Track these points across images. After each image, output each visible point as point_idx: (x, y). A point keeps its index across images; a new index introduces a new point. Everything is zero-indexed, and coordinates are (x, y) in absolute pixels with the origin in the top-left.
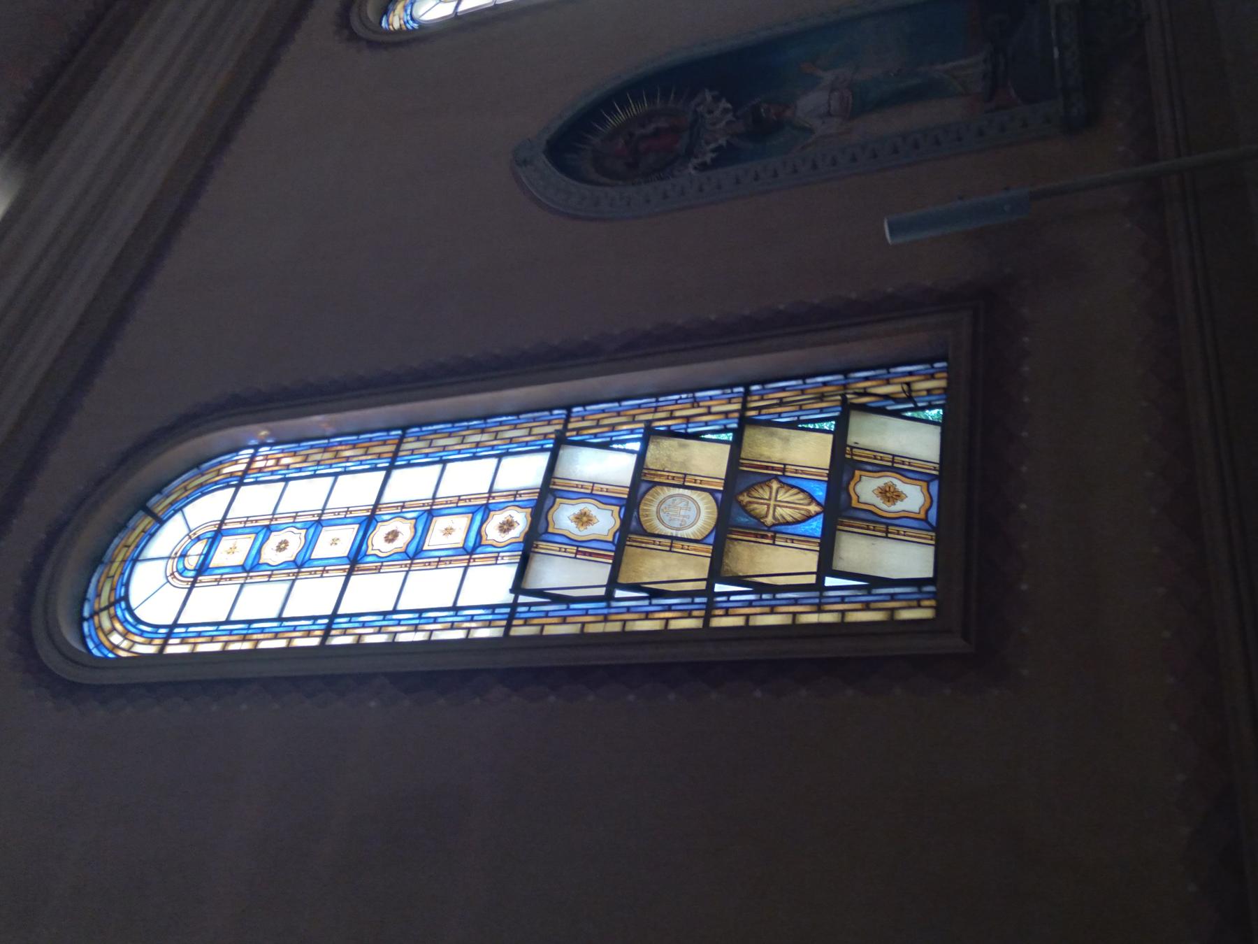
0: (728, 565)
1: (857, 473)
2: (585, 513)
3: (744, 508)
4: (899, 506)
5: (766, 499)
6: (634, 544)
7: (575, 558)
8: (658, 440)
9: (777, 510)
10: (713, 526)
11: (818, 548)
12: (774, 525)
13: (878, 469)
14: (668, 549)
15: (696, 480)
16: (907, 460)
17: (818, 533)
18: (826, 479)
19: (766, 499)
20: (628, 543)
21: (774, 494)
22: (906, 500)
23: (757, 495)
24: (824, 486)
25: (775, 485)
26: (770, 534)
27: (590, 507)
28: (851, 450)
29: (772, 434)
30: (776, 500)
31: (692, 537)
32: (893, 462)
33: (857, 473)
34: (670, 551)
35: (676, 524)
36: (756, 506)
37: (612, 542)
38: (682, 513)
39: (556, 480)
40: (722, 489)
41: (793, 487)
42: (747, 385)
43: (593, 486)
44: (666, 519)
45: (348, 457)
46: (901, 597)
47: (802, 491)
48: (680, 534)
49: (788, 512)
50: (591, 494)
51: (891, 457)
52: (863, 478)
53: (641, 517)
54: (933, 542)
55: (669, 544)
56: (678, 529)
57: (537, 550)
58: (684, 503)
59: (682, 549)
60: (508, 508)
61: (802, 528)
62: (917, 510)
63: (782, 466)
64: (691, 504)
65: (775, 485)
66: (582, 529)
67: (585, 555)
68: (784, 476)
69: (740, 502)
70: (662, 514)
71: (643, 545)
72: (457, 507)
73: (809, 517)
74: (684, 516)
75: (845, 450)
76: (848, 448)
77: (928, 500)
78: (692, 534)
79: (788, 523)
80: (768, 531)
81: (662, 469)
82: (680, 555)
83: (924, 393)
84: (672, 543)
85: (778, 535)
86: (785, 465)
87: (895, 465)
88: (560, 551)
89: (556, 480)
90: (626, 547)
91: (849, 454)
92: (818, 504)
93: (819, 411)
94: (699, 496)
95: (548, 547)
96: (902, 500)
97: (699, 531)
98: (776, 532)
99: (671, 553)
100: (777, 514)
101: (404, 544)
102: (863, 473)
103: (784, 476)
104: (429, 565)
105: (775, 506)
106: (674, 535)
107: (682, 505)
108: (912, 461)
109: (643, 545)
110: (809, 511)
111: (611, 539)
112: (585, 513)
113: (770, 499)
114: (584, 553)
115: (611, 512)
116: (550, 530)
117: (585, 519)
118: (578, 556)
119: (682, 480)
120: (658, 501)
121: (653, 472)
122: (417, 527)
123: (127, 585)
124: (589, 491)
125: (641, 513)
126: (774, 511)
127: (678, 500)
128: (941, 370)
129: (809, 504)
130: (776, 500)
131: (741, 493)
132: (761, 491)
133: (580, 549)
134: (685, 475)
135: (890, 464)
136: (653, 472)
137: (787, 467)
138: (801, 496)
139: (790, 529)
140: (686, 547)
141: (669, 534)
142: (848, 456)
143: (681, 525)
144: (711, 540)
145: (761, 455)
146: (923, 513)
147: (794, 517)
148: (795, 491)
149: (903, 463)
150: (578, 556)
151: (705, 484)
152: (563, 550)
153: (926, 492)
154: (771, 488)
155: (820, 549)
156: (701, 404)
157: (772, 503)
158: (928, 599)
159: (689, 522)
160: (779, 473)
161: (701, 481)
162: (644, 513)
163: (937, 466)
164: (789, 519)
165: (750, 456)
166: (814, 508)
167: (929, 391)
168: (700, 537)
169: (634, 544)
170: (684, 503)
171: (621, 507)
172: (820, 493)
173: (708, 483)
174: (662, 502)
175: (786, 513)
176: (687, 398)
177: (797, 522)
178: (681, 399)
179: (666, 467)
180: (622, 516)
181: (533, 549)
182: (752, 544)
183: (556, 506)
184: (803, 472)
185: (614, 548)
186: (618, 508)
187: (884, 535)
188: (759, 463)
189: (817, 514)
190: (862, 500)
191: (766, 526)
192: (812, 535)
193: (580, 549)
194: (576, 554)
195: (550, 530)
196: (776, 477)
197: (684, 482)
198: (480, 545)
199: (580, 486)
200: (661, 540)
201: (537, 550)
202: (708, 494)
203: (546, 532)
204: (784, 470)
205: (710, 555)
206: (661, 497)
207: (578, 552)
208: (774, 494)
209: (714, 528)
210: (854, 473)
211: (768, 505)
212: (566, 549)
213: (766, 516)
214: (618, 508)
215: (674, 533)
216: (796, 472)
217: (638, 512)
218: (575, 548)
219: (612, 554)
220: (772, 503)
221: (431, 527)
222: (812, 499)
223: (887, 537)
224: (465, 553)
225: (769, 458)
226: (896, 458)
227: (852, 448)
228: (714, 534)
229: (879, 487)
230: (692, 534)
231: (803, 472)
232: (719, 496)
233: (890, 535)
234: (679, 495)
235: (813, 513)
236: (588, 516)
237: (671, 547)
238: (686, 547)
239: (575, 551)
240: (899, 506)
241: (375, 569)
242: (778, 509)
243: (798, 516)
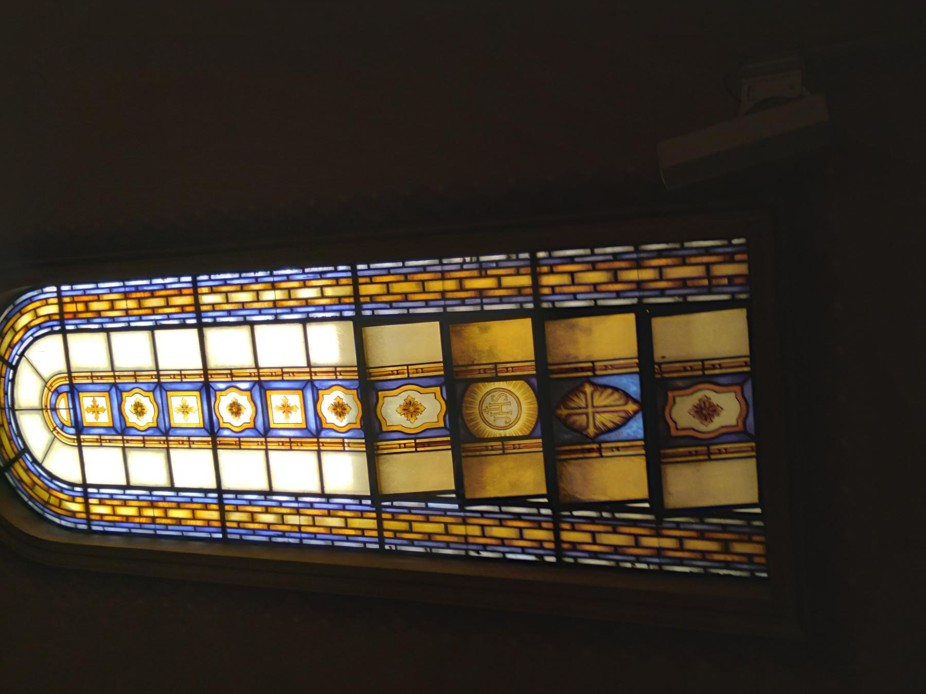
0: (564, 490)
1: (670, 394)
2: (410, 402)
3: (565, 422)
4: (718, 422)
5: (584, 408)
6: (470, 454)
7: (416, 451)
8: (458, 328)
9: (596, 418)
10: (536, 416)
11: (643, 452)
12: (597, 435)
13: (688, 382)
14: (501, 452)
15: (507, 368)
16: (717, 362)
17: (641, 434)
18: (637, 370)
19: (584, 408)
20: (463, 454)
21: (589, 400)
22: (723, 414)
23: (573, 405)
24: (636, 379)
25: (588, 389)
26: (595, 446)
27: (411, 393)
28: (660, 368)
29: (572, 327)
30: (593, 407)
31: (520, 434)
32: (704, 369)
33: (670, 394)
34: (504, 454)
35: (501, 423)
36: (576, 418)
37: (445, 427)
38: (504, 409)
39: (371, 370)
40: (534, 372)
41: (605, 387)
42: (559, 563)
43: (408, 369)
44: (490, 419)
45: (153, 308)
46: (732, 529)
47: (616, 389)
48: (508, 433)
49: (607, 418)
50: (408, 378)
51: (700, 363)
52: (678, 399)
53: (467, 423)
54: (754, 454)
55: (501, 447)
56: (504, 428)
57: (380, 452)
58: (503, 397)
59: (514, 449)
60: (334, 387)
61: (626, 432)
62: (733, 395)
63: (590, 364)
64: (510, 398)
65: (588, 389)
66: (412, 420)
67: (424, 447)
68: (595, 376)
69: (559, 417)
70: (485, 414)
71: (478, 453)
72: (283, 381)
73: (627, 419)
74: (507, 413)
75: (654, 368)
76: (656, 367)
77: (744, 407)
78: (519, 430)
79: (610, 430)
80: (594, 442)
81: (471, 363)
82: (513, 455)
83: (725, 281)
84: (503, 445)
85: (603, 445)
86: (593, 362)
87: (707, 372)
88: (400, 448)
89: (371, 370)
90: (463, 459)
91: (658, 373)
92: (635, 401)
93: (614, 295)
94: (515, 386)
95: (389, 446)
96: (718, 415)
97: (524, 425)
98: (600, 443)
99: (505, 456)
100: (598, 423)
101: (250, 419)
102: (676, 393)
103: (595, 376)
104: (283, 445)
105: (594, 413)
106: (503, 435)
107: (501, 400)
108: (722, 361)
109: (478, 453)
110: (626, 412)
111: (443, 425)
112: (410, 402)
113: (587, 407)
114: (423, 445)
115: (433, 395)
116: (384, 429)
117: (412, 409)
118: (418, 449)
119: (494, 371)
120: (479, 415)
121: (463, 368)
122: (254, 399)
123: (20, 435)
124: (406, 376)
125: (466, 419)
126: (594, 419)
127: (496, 394)
128: (740, 249)
129: (626, 404)
130: (593, 407)
131: (558, 407)
132: (576, 399)
133: (418, 441)
134: (496, 364)
135: (700, 373)
136: (463, 368)
137: (597, 364)
138: (616, 396)
139: (613, 436)
140: (518, 446)
141: (498, 436)
142: (658, 376)
143: (506, 423)
144: (538, 432)
145: (568, 356)
146: (740, 424)
147: (613, 420)
148: (609, 391)
149: (714, 367)
150: (419, 449)
151: (517, 371)
152: (403, 446)
153: (740, 398)
154: (585, 393)
155: (646, 452)
156: (490, 272)
157: (590, 410)
158: (758, 534)
159: (513, 417)
160: (590, 374)
161: (512, 368)
162: (469, 418)
163: (747, 359)
164: (610, 425)
165: (557, 360)
166: (631, 407)
167: (731, 278)
168: (528, 432)
169: (470, 454)
170: (503, 397)
171: (441, 386)
172: (634, 388)
173: (520, 368)
174: (482, 402)
175: (604, 419)
176: (471, 263)
177: (618, 427)
178: (464, 262)
179: (475, 360)
180: (445, 397)
181: (375, 452)
182: (581, 461)
183: (380, 401)
184: (613, 367)
185: (448, 433)
186: (438, 388)
187: (706, 457)
188: (567, 366)
189: (636, 413)
190: (680, 426)
191: (590, 438)
192: (635, 438)
193: (418, 441)
194: (416, 447)
195: (384, 429)
196: (588, 380)
197: (496, 373)
198: (322, 429)
199: (396, 372)
200: (493, 444)
201: (380, 452)
202: (523, 381)
203: (382, 432)
204: (593, 369)
205: (541, 449)
206: (479, 397)
207: (417, 445)
208: (589, 400)
209: (537, 419)
210: (667, 395)
211: (587, 414)
212: (405, 444)
213: (588, 426)
214: (438, 388)
215: (502, 433)
216: (606, 368)
217: (463, 419)
218: (413, 441)
219: (449, 439)
220: (590, 410)
221: (269, 402)
222: (628, 397)
223: (710, 460)
224: (311, 435)
225: (576, 357)
226: (706, 363)
227: (659, 364)
228: (539, 425)
229: (695, 406)
230: (519, 430)
231: (613, 367)
232: (534, 381)
233: (713, 457)
234: (495, 390)
235: (631, 412)
236: (414, 405)
237: (503, 449)
238: (518, 446)
239: (414, 444)
240: (718, 422)
241: (236, 445)
242: (597, 416)
243: (616, 418)
